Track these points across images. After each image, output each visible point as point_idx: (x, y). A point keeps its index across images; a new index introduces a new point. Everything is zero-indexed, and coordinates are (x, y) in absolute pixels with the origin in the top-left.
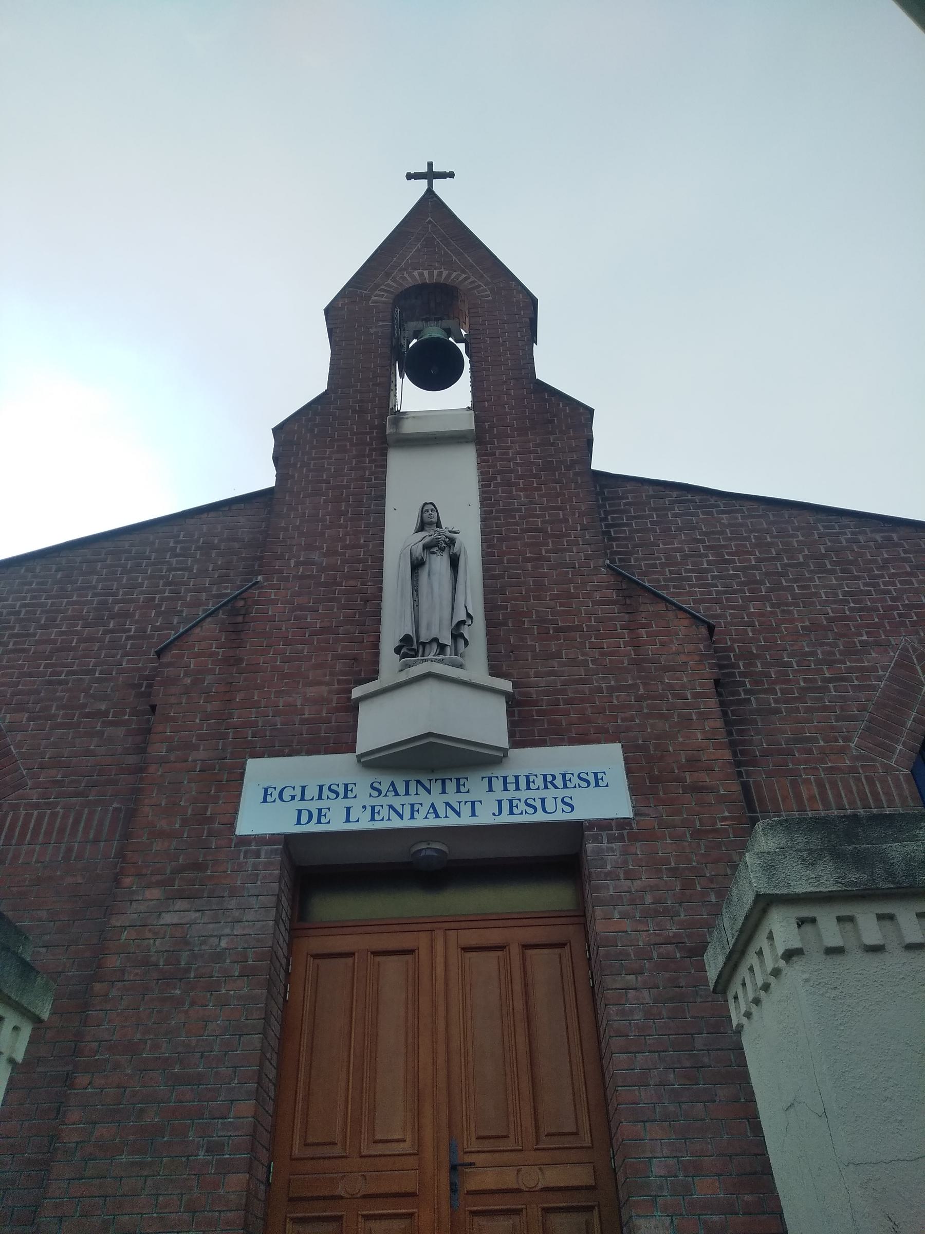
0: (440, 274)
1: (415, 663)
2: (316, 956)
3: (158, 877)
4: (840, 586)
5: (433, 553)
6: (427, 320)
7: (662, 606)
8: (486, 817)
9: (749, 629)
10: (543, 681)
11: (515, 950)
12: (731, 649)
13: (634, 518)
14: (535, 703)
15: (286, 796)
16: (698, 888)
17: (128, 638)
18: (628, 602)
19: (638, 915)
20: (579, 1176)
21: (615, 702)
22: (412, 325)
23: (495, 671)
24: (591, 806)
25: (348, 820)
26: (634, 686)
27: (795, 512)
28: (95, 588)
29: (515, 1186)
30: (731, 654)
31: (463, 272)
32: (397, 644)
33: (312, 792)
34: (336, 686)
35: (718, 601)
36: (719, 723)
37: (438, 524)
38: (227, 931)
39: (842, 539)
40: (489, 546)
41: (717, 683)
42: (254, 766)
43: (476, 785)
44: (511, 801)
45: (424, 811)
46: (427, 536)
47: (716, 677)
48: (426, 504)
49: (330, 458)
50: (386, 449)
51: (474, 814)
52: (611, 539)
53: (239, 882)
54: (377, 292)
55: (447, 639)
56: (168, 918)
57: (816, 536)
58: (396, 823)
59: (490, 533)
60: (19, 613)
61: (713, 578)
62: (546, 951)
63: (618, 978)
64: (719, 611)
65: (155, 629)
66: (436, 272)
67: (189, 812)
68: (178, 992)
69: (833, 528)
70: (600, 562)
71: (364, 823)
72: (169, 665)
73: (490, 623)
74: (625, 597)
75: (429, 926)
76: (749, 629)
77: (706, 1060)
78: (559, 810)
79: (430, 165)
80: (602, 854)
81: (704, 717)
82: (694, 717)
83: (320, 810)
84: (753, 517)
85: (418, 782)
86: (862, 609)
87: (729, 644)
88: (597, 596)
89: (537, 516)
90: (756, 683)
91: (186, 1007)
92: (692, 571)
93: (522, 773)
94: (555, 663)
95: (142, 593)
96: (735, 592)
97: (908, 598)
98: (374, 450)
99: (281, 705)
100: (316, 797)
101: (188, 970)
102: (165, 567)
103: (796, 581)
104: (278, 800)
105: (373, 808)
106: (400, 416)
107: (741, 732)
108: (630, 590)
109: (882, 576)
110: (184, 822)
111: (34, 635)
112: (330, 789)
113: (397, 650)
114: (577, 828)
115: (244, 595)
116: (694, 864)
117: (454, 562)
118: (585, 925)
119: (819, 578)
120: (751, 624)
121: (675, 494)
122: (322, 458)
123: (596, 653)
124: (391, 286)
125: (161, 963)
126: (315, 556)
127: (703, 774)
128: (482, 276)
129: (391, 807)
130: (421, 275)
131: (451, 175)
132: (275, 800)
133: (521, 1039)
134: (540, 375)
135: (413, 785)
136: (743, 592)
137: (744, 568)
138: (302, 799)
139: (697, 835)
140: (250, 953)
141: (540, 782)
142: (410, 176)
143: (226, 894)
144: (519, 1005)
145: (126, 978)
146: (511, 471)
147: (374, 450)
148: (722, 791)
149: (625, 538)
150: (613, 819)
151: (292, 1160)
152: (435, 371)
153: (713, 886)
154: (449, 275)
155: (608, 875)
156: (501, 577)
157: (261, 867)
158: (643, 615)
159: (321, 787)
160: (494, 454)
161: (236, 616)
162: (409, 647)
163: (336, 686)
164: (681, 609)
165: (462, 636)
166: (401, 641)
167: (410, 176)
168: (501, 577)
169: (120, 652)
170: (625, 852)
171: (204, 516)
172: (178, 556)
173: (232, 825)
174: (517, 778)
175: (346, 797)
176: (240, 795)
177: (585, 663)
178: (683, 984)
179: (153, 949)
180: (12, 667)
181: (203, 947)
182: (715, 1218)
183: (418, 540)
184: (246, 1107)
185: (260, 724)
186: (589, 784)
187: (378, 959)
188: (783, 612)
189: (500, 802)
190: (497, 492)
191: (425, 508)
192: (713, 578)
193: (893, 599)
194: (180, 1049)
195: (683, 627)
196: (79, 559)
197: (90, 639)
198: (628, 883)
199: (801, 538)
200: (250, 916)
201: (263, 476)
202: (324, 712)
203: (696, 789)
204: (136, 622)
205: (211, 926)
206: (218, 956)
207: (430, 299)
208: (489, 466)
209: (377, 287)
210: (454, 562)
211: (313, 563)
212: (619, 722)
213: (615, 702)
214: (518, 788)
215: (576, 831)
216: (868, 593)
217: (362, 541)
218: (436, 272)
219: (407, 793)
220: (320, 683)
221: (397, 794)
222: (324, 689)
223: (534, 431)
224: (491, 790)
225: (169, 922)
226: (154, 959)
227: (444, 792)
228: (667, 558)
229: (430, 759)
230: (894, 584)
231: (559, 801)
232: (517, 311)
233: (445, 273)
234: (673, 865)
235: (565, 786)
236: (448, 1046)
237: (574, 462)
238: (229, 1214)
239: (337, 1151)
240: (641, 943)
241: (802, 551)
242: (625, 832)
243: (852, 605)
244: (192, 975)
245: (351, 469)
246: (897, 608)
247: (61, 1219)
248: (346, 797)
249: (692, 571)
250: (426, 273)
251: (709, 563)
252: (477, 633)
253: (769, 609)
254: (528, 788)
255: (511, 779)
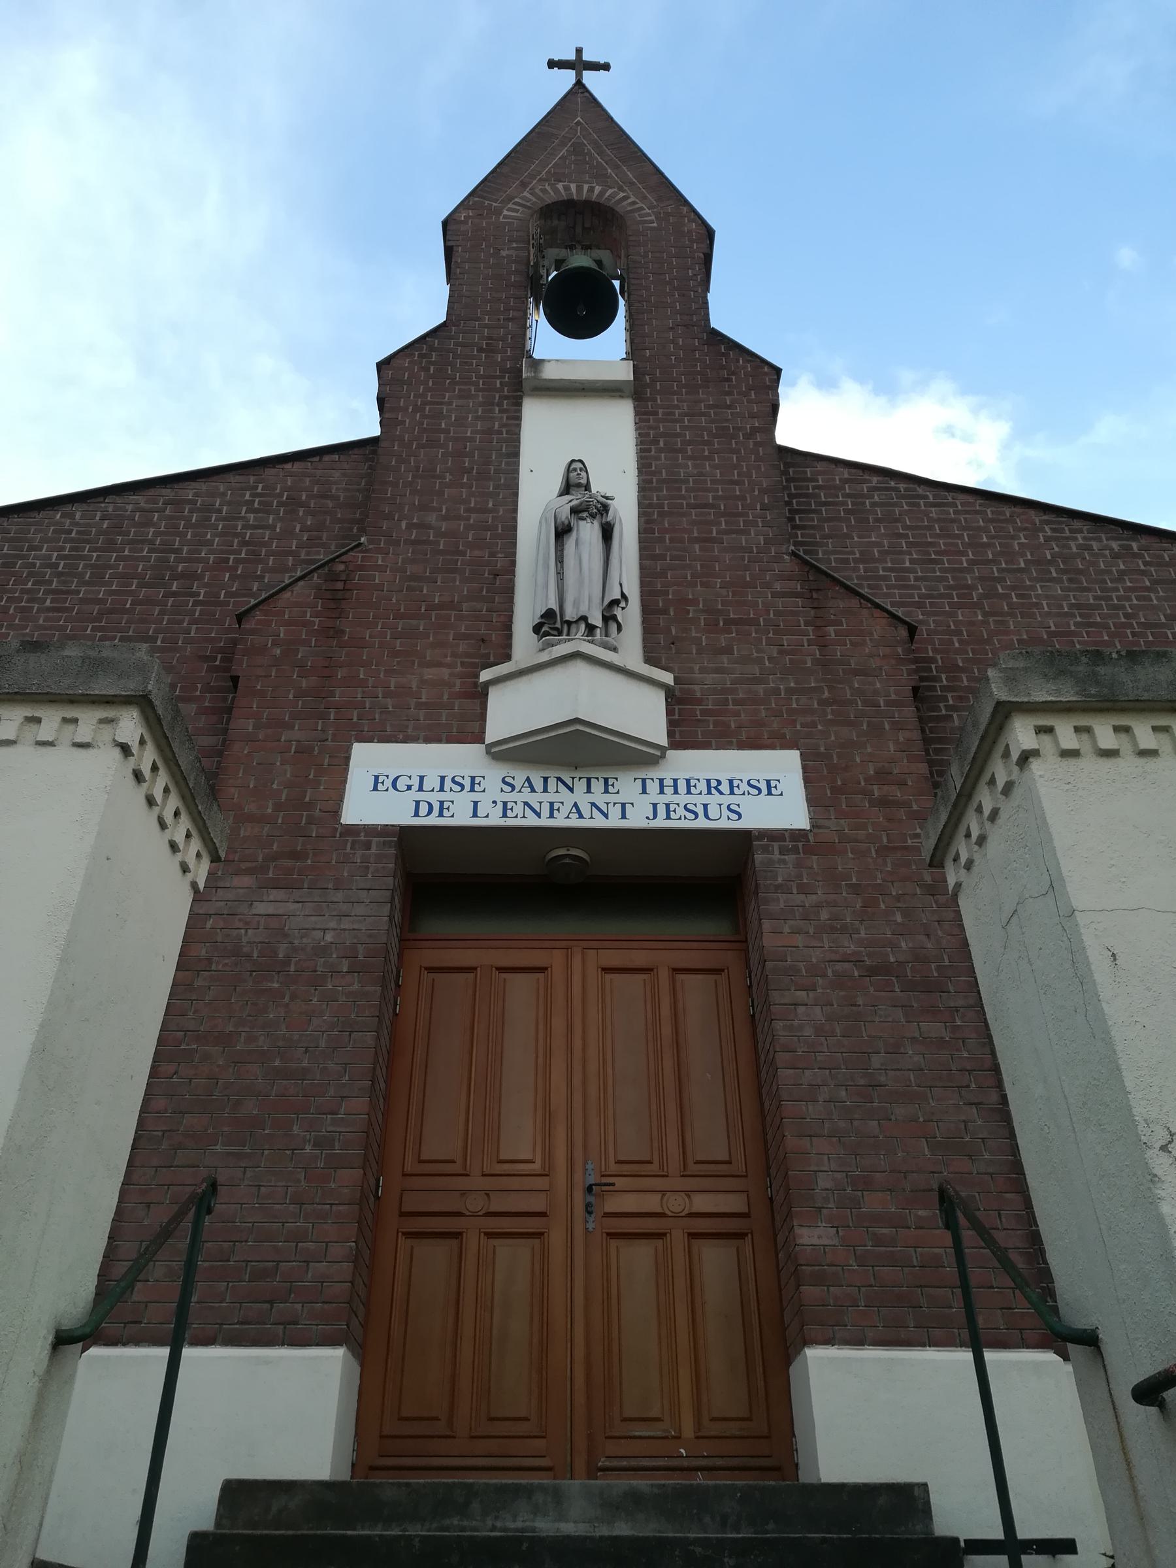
0: (591, 190)
1: (559, 642)
2: (430, 969)
3: (248, 865)
4: (1067, 598)
5: (583, 519)
6: (572, 248)
7: (854, 602)
8: (638, 819)
9: (955, 639)
10: (710, 678)
11: (664, 975)
12: (933, 660)
13: (825, 504)
14: (699, 702)
15: (401, 784)
16: (883, 906)
17: (196, 603)
18: (815, 595)
19: (811, 932)
20: (732, 1203)
21: (794, 705)
22: (553, 253)
23: (650, 658)
24: (760, 814)
25: (475, 815)
26: (819, 689)
27: (1018, 510)
28: (152, 542)
29: (659, 1210)
30: (933, 666)
31: (621, 189)
32: (537, 621)
33: (432, 782)
34: (459, 669)
35: (920, 605)
36: (916, 735)
37: (587, 487)
38: (332, 925)
39: (1072, 544)
40: (647, 522)
41: (915, 690)
42: (360, 751)
43: (627, 785)
44: (668, 806)
45: (565, 810)
46: (575, 499)
47: (913, 684)
48: (573, 461)
49: (450, 404)
50: (521, 398)
51: (624, 817)
52: (794, 527)
53: (346, 874)
54: (510, 206)
55: (596, 620)
56: (261, 908)
57: (1042, 540)
58: (532, 821)
59: (650, 506)
60: (57, 565)
61: (917, 579)
62: (700, 977)
63: (787, 993)
64: (921, 617)
65: (229, 594)
66: (586, 187)
67: (284, 797)
68: (276, 985)
69: (1062, 531)
70: (784, 548)
71: (493, 818)
72: (253, 632)
73: (648, 611)
74: (811, 590)
75: (564, 944)
76: (955, 639)
77: (883, 1079)
78: (724, 817)
79: (579, 51)
80: (770, 867)
81: (898, 726)
82: (887, 727)
83: (442, 803)
84: (967, 512)
85: (559, 779)
86: (1090, 625)
87: (931, 654)
88: (778, 586)
89: (708, 490)
90: (961, 698)
91: (287, 1000)
92: (891, 570)
93: (681, 776)
94: (725, 659)
95: (210, 552)
96: (942, 596)
97: (1144, 616)
98: (506, 397)
99: (392, 685)
100: (437, 788)
101: (288, 963)
102: (240, 524)
103: (1013, 588)
104: (391, 788)
105: (505, 804)
106: (537, 364)
107: (938, 751)
108: (817, 580)
109: (1117, 590)
110: (278, 807)
111: (78, 592)
112: (453, 781)
113: (537, 629)
114: (745, 838)
115: (344, 558)
116: (879, 881)
117: (607, 533)
118: (746, 951)
119: (1041, 587)
120: (958, 633)
121: (875, 479)
122: (442, 403)
123: (774, 651)
124: (529, 200)
125: (255, 955)
126: (432, 518)
127: (893, 787)
128: (645, 198)
129: (526, 804)
130: (567, 188)
131: (606, 67)
132: (390, 785)
133: (668, 1064)
134: (716, 323)
135: (552, 783)
136: (951, 596)
137: (953, 570)
138: (421, 789)
139: (884, 851)
140: (360, 948)
141: (702, 786)
142: (552, 64)
143: (330, 886)
144: (667, 1030)
145: (213, 968)
146: (677, 435)
147: (506, 397)
148: (915, 807)
149: (813, 527)
150: (786, 830)
151: (404, 1175)
152: (580, 313)
153: (899, 905)
154: (602, 193)
155: (778, 888)
156: (662, 557)
157: (372, 860)
158: (832, 611)
159: (443, 778)
160: (656, 414)
161: (336, 585)
162: (550, 624)
163: (459, 669)
164: (877, 606)
165: (614, 618)
166: (542, 617)
167: (552, 64)
168: (662, 557)
169: (187, 618)
170: (799, 865)
171: (289, 466)
172: (256, 511)
173: (337, 812)
174: (675, 781)
175: (472, 790)
176: (345, 781)
177: (760, 661)
178: (861, 1002)
179: (245, 940)
180: (50, 628)
181: (304, 940)
182: (884, 1231)
183: (565, 505)
184: (360, 1104)
185: (367, 706)
186: (762, 791)
187: (504, 975)
188: (996, 622)
189: (655, 806)
190: (658, 459)
191: (574, 466)
192: (917, 579)
193: (1126, 616)
194: (280, 1044)
195: (879, 627)
196: (130, 507)
197: (149, 602)
198: (802, 897)
199: (1023, 540)
200: (359, 910)
201: (365, 423)
202: (446, 697)
203: (884, 803)
204: (206, 585)
205: (313, 918)
206: (322, 950)
207: (573, 228)
208: (650, 428)
209: (510, 199)
210: (607, 533)
211: (429, 527)
212: (798, 727)
213: (794, 705)
214: (676, 792)
215: (742, 843)
216: (1100, 607)
217: (490, 505)
218: (586, 187)
219: (545, 790)
220: (439, 665)
221: (533, 790)
222: (445, 672)
223: (707, 393)
224: (644, 791)
225: (262, 912)
226: (245, 949)
227: (589, 791)
228: (861, 553)
229: (577, 749)
230: (1129, 599)
231: (724, 808)
232: (692, 243)
233: (598, 189)
234: (854, 881)
235: (732, 793)
236: (584, 1067)
237: (754, 430)
238: (341, 1208)
239: (456, 1168)
240: (814, 960)
241: (1023, 555)
242: (800, 844)
243: (1078, 619)
244: (292, 969)
245: (477, 418)
246: (1131, 626)
247: (148, 1205)
248: (472, 790)
249: (891, 570)
250: (573, 187)
251: (912, 561)
252: (631, 615)
253: (980, 617)
254: (689, 792)
255: (668, 782)
